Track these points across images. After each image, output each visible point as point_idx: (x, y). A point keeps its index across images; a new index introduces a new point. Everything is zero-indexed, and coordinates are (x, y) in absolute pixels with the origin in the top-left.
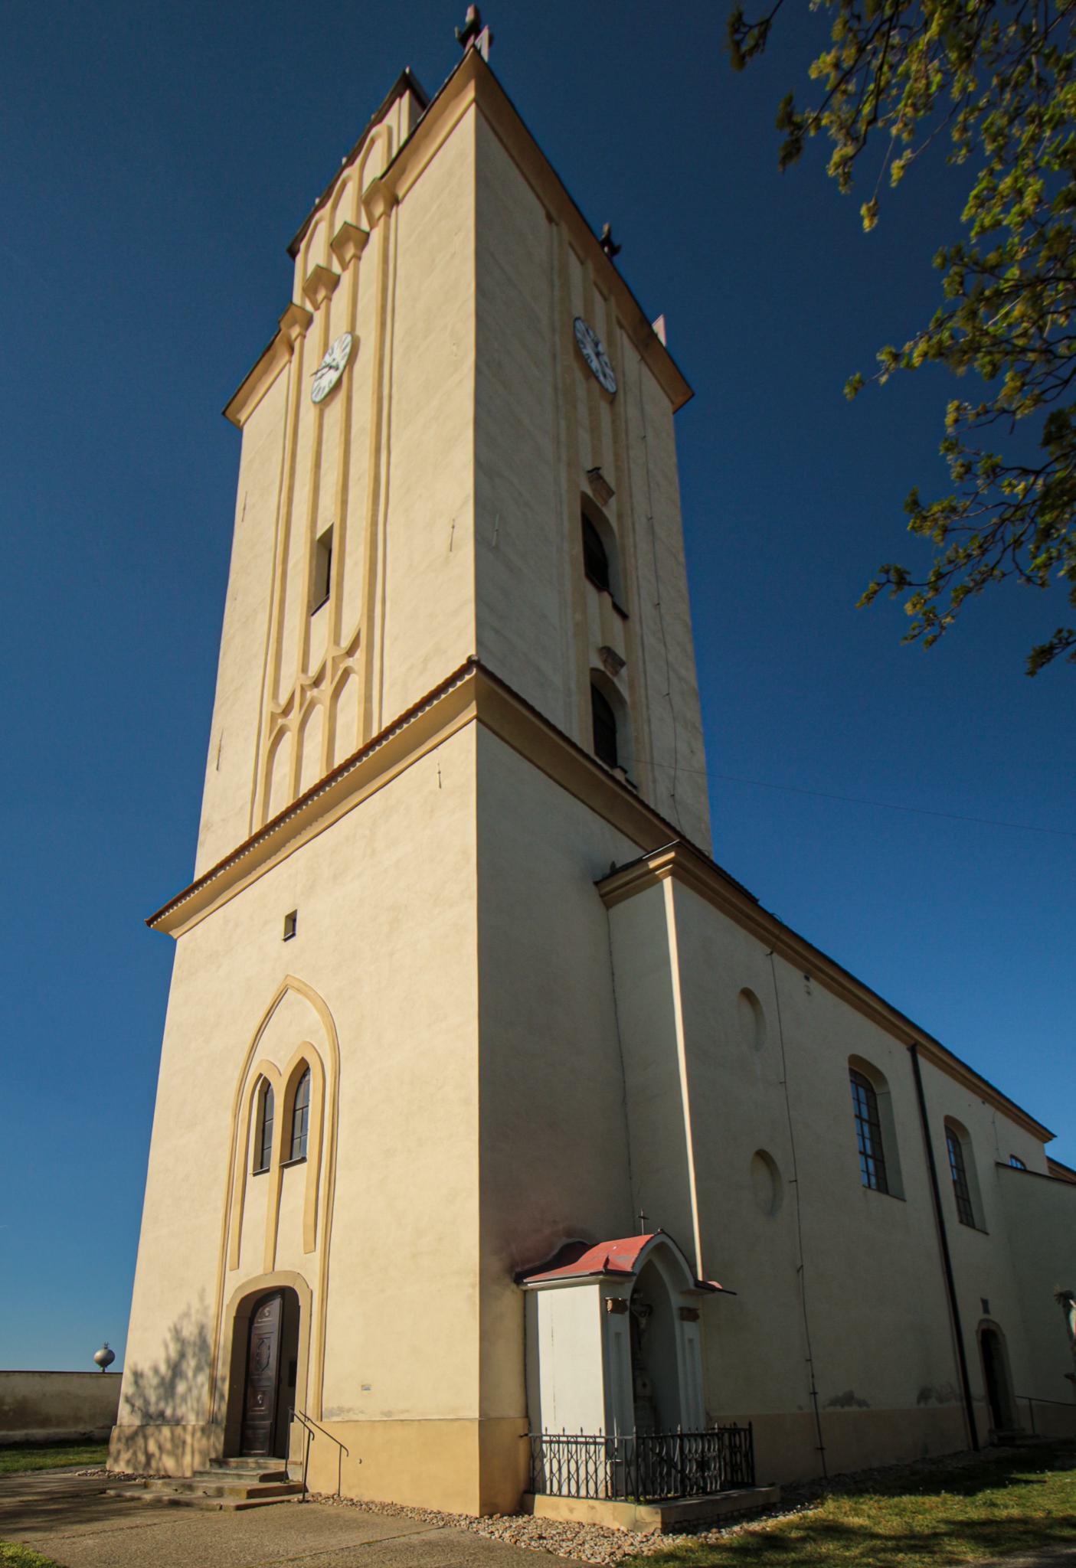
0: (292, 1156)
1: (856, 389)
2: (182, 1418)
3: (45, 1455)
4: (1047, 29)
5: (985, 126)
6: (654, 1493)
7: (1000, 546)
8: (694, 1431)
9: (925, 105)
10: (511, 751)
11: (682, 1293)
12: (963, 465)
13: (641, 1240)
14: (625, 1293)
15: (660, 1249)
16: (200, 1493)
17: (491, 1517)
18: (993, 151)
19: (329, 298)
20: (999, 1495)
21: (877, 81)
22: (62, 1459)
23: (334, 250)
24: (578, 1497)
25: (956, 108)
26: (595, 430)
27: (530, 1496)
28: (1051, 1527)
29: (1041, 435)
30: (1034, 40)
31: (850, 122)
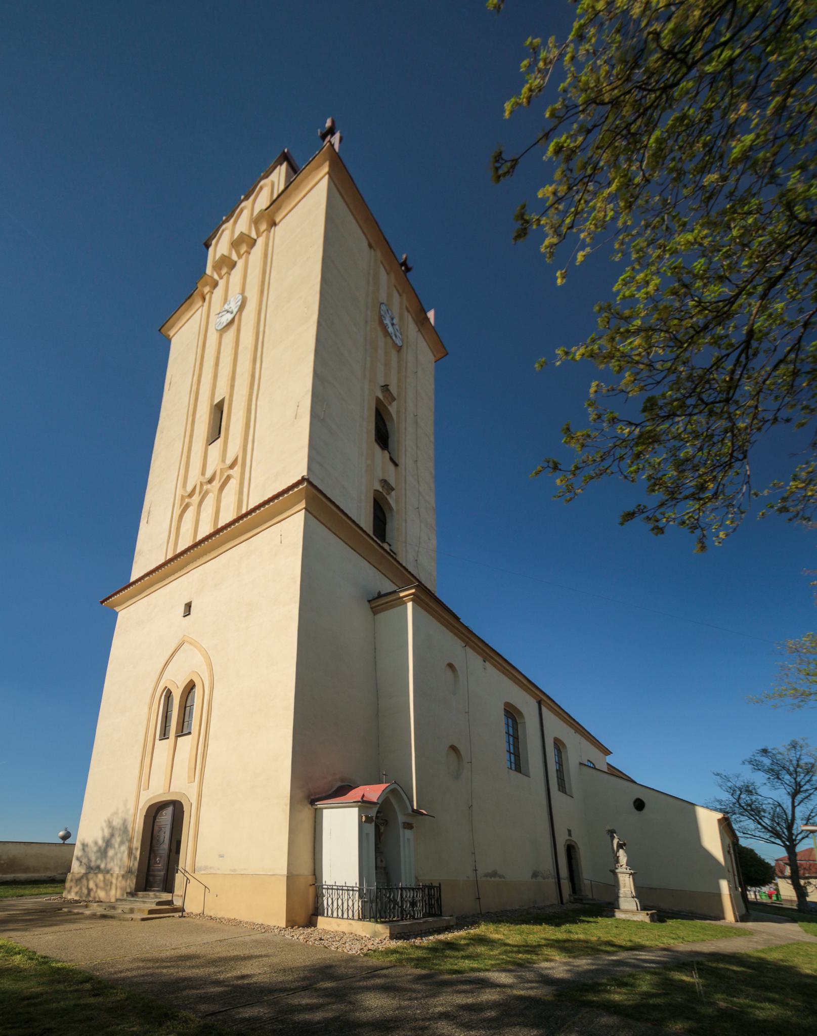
0: (183, 730)
1: (542, 366)
2: (111, 869)
3: (25, 888)
4: (676, 203)
5: (634, 244)
6: (386, 918)
7: (612, 458)
8: (408, 886)
9: (602, 226)
10: (324, 528)
11: (405, 815)
12: (596, 415)
13: (383, 786)
14: (373, 813)
15: (393, 791)
16: (120, 911)
17: (292, 927)
18: (636, 258)
19: (229, 273)
21: (577, 207)
22: (35, 891)
23: (233, 247)
24: (343, 918)
25: (619, 232)
26: (387, 365)
28: (600, 945)
29: (641, 407)
30: (668, 207)
31: (557, 225)
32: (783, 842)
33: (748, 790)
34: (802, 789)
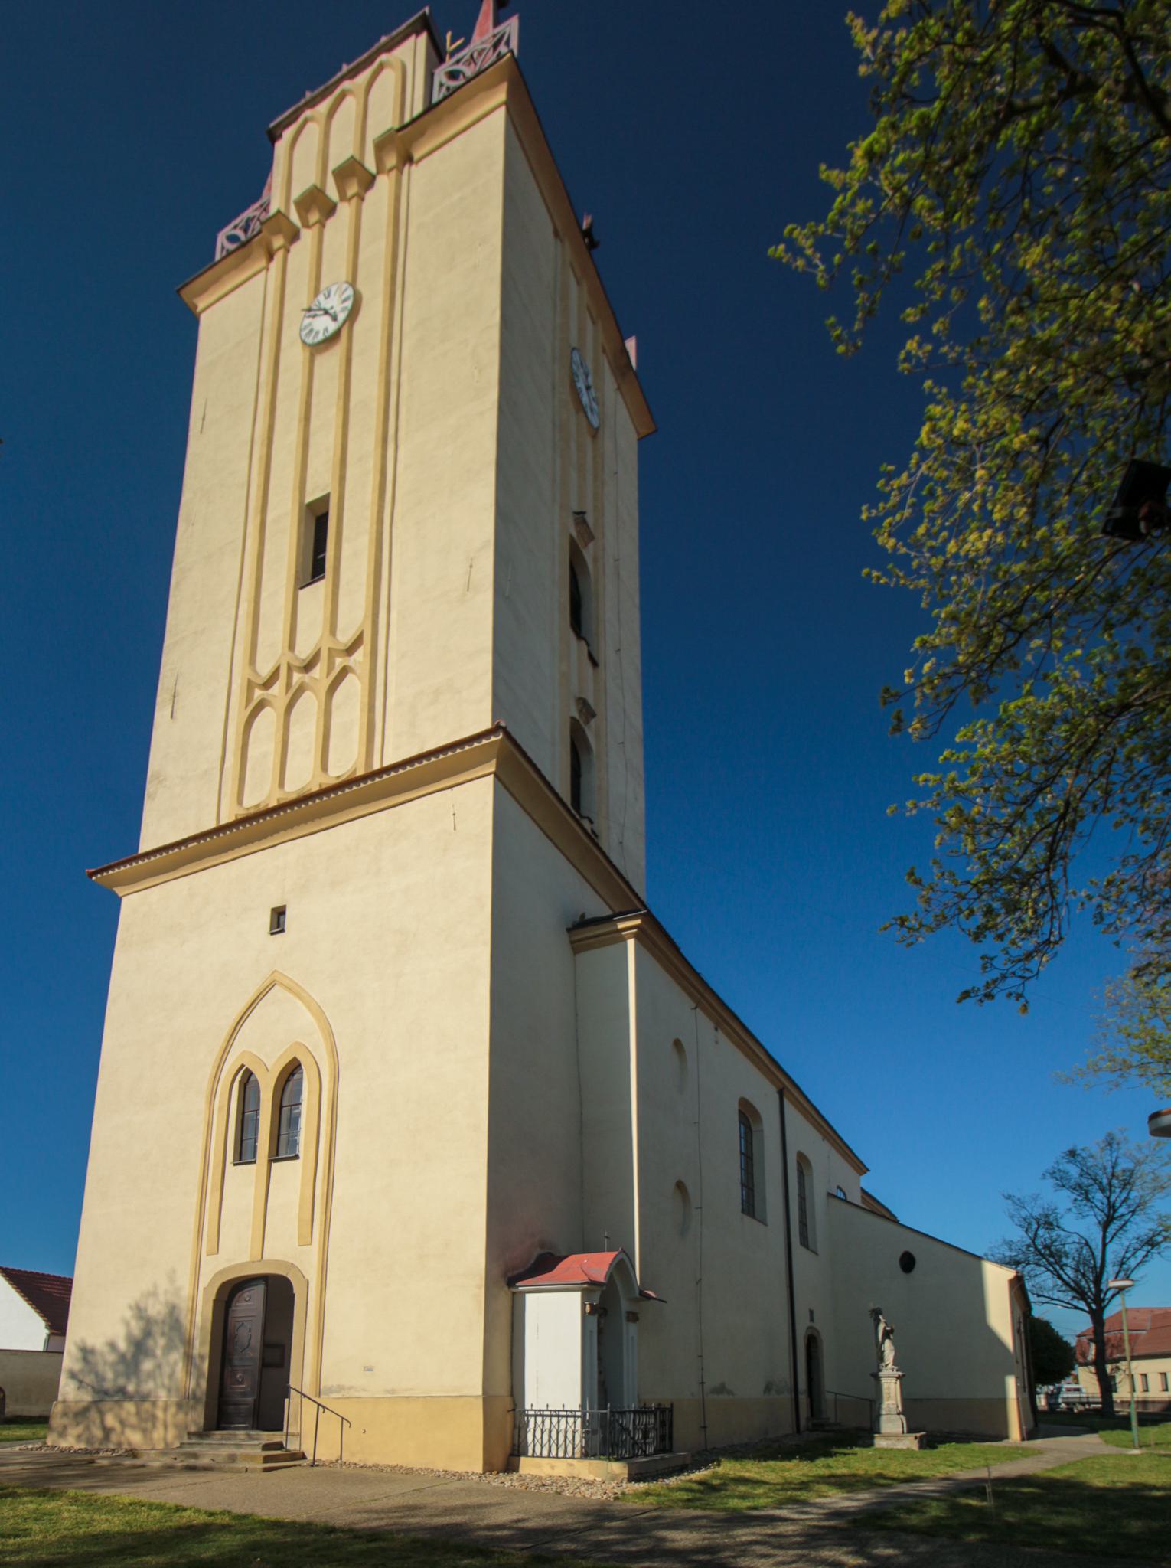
0: (283, 1148)
13: (614, 1254)
20: (830, 1461)
27: (516, 1458)
32: (1088, 1305)
33: (1048, 1222)
34: (1117, 1214)
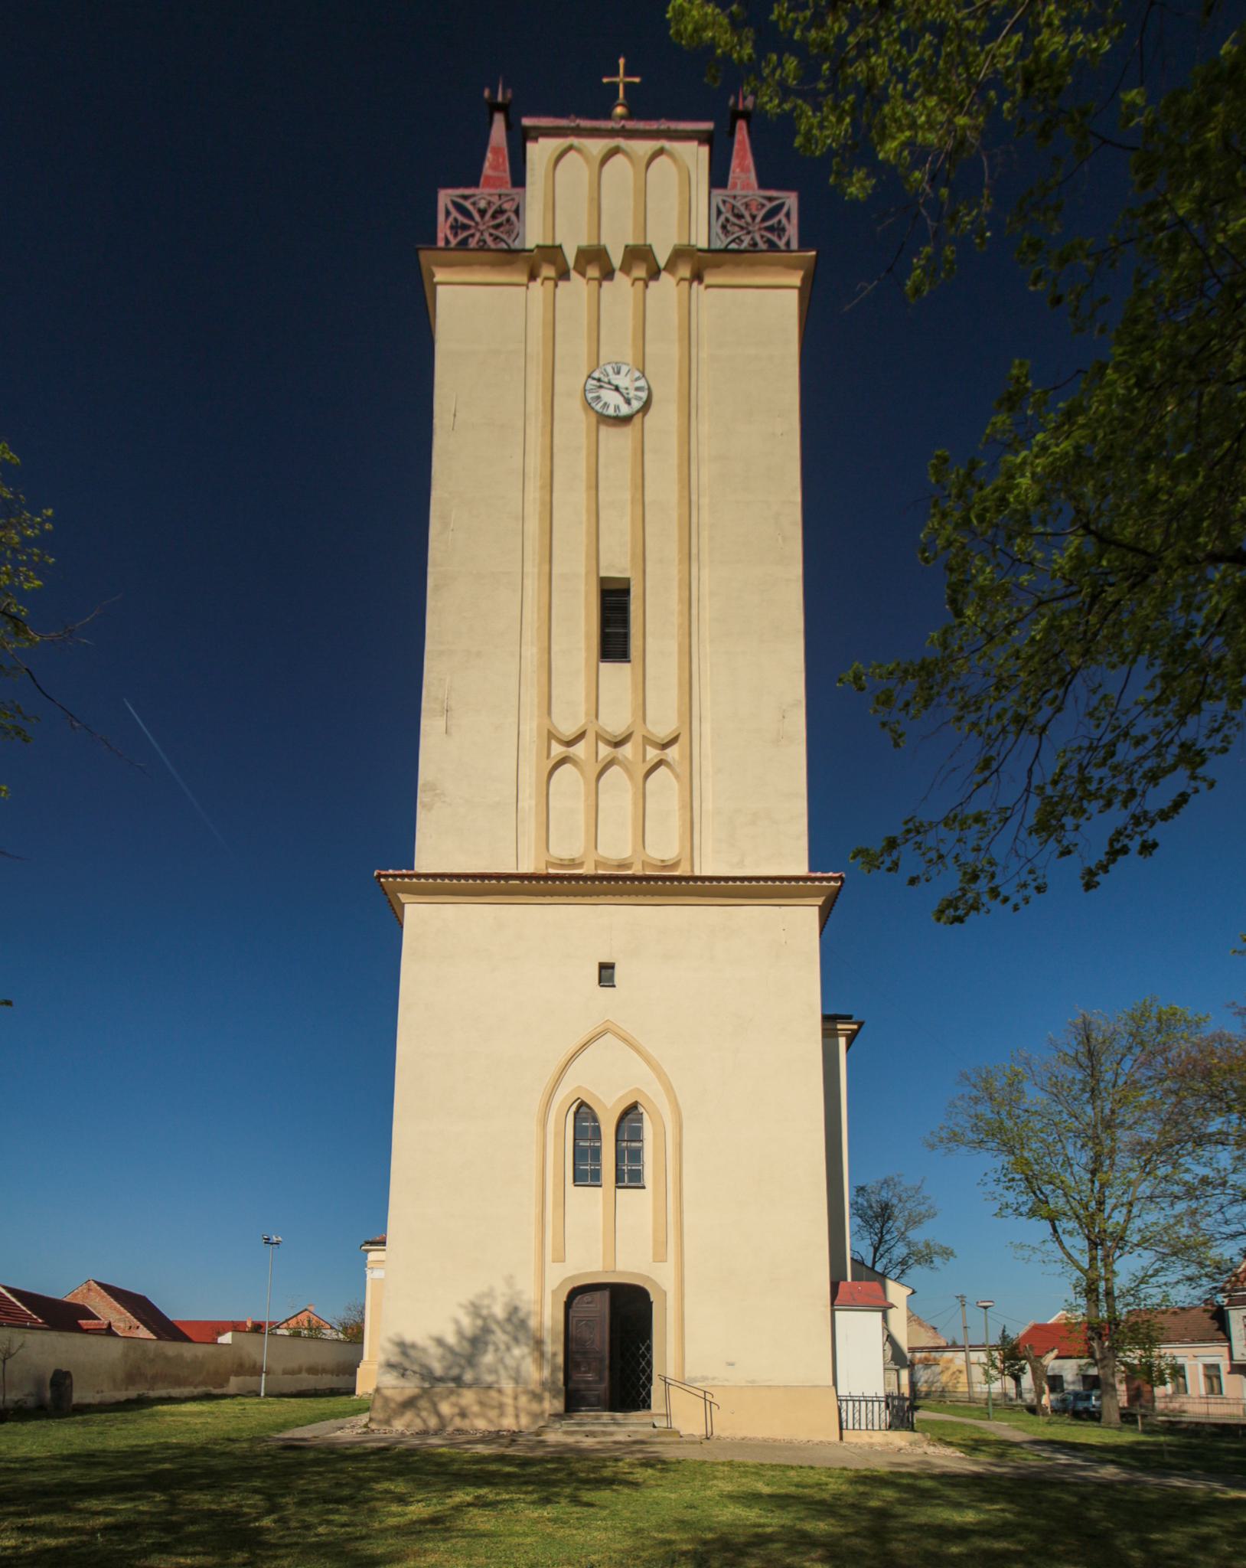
0: (629, 1176)
